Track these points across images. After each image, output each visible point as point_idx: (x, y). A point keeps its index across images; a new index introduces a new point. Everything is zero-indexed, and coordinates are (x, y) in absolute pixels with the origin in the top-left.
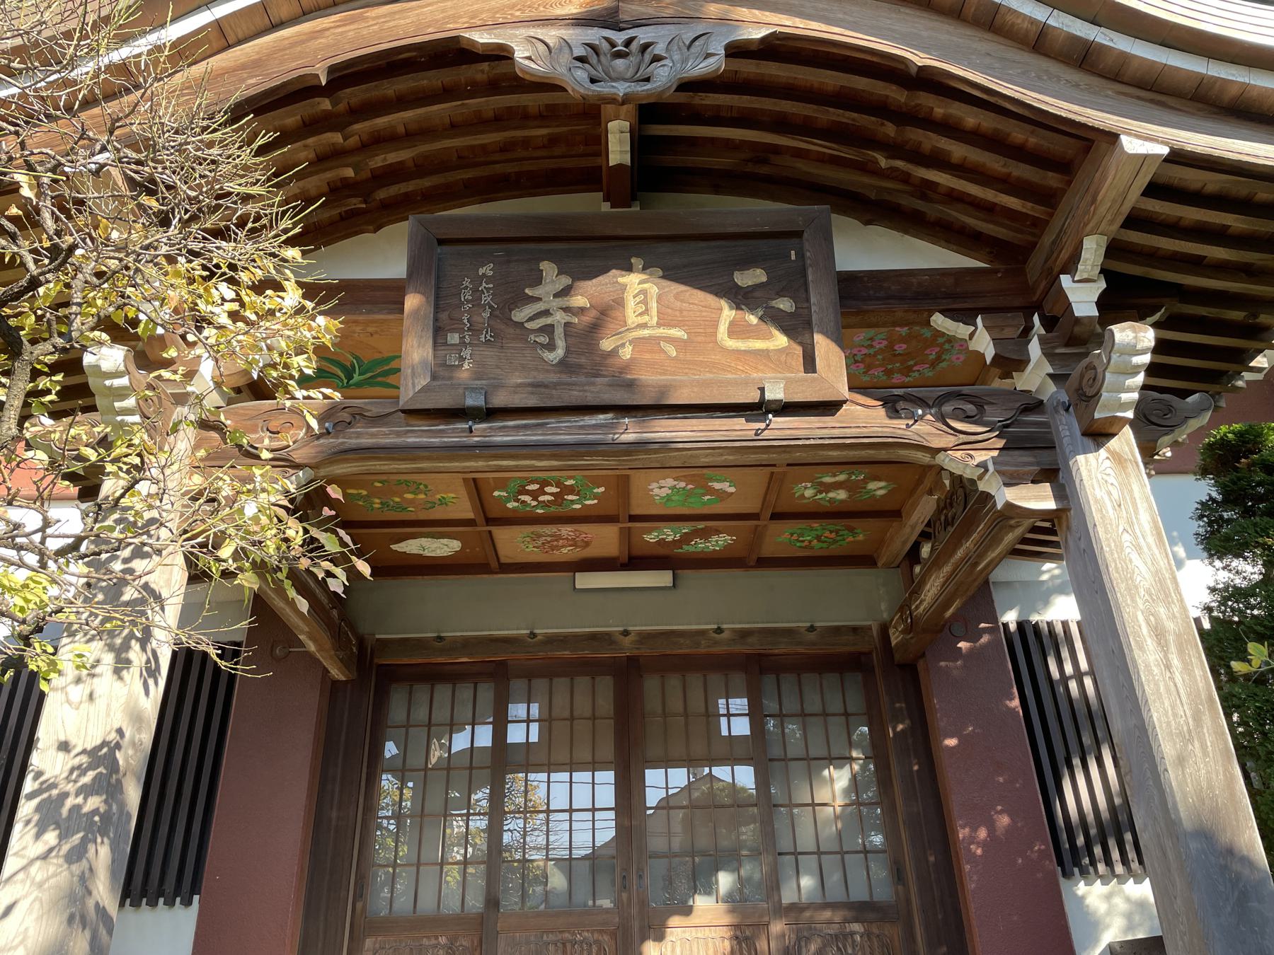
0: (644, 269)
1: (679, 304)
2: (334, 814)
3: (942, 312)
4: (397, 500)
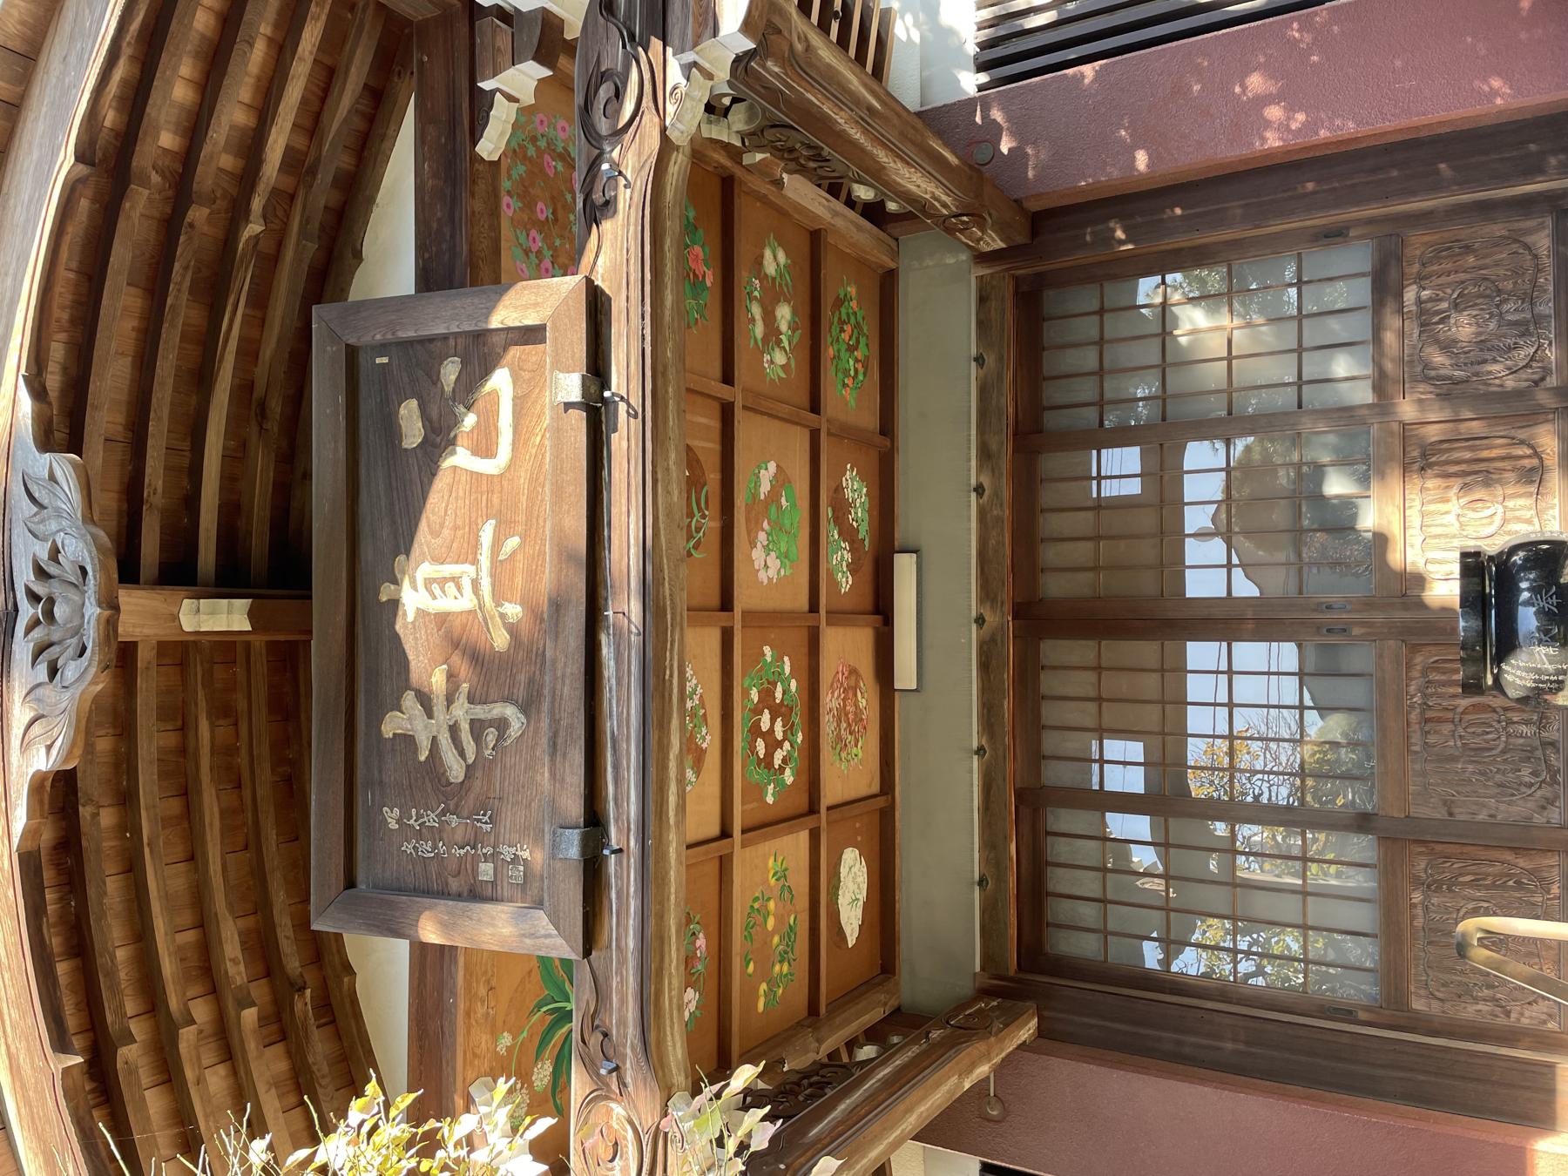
0: (396, 582)
1: (446, 532)
2: (1229, 1046)
3: (475, 143)
4: (776, 939)
